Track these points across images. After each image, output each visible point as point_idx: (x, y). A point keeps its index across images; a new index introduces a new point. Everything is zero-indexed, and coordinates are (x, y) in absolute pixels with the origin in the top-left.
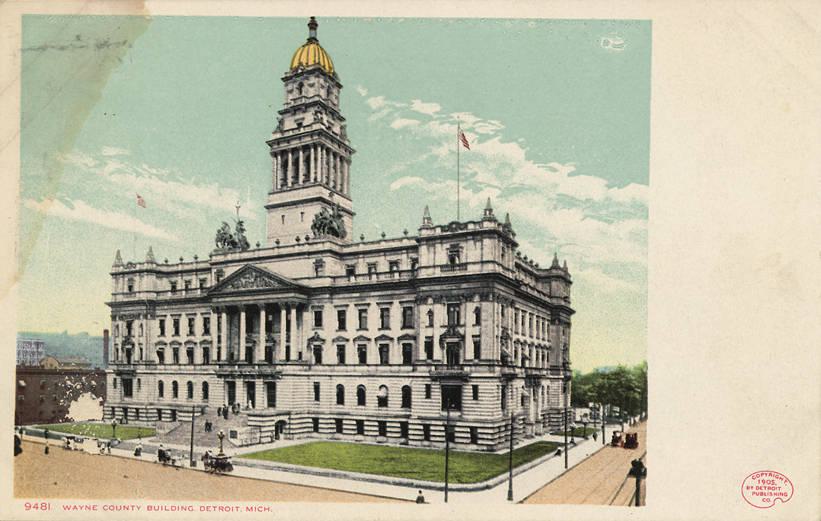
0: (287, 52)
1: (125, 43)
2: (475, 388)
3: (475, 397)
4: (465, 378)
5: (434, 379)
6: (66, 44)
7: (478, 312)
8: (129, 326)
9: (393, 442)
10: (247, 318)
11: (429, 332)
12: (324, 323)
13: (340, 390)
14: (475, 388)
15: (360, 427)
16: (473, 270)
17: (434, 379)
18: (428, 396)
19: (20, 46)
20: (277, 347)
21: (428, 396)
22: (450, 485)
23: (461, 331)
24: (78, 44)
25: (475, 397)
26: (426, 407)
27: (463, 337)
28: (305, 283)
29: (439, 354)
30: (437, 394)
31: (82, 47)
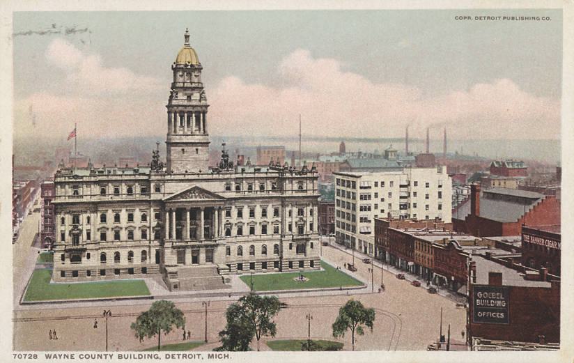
0: (172, 51)
1: (86, 30)
2: (312, 243)
3: (312, 247)
4: (307, 240)
5: (66, 251)
6: (46, 30)
7: (89, 219)
8: (76, 220)
9: (273, 271)
10: (176, 215)
11: (88, 227)
12: (107, 220)
13: (240, 249)
14: (312, 243)
15: (252, 266)
16: (85, 200)
17: (293, 240)
18: (291, 248)
19: (11, 32)
20: (199, 228)
21: (291, 248)
22: (343, 288)
23: (80, 227)
24: (54, 30)
25: (312, 247)
26: (289, 254)
27: (81, 231)
28: (220, 194)
29: (295, 229)
30: (294, 249)
31: (56, 32)
